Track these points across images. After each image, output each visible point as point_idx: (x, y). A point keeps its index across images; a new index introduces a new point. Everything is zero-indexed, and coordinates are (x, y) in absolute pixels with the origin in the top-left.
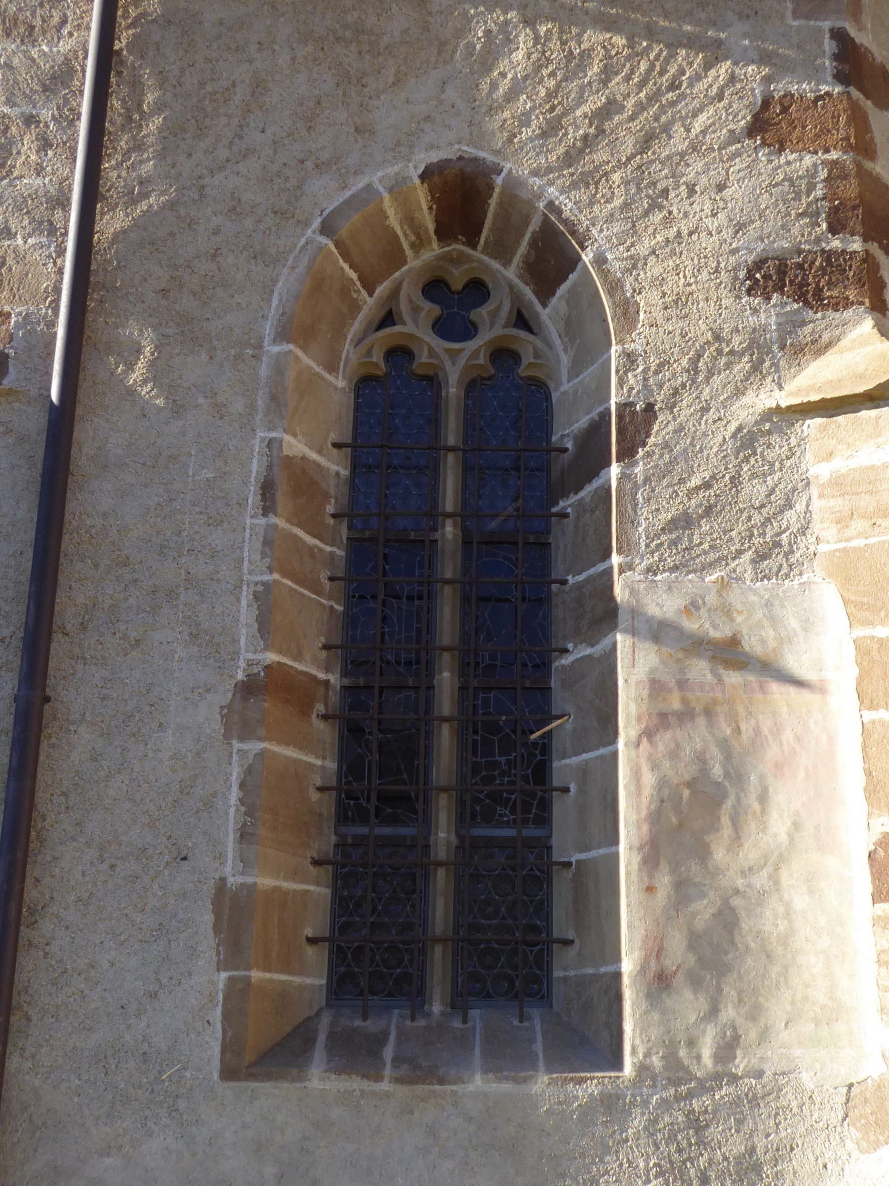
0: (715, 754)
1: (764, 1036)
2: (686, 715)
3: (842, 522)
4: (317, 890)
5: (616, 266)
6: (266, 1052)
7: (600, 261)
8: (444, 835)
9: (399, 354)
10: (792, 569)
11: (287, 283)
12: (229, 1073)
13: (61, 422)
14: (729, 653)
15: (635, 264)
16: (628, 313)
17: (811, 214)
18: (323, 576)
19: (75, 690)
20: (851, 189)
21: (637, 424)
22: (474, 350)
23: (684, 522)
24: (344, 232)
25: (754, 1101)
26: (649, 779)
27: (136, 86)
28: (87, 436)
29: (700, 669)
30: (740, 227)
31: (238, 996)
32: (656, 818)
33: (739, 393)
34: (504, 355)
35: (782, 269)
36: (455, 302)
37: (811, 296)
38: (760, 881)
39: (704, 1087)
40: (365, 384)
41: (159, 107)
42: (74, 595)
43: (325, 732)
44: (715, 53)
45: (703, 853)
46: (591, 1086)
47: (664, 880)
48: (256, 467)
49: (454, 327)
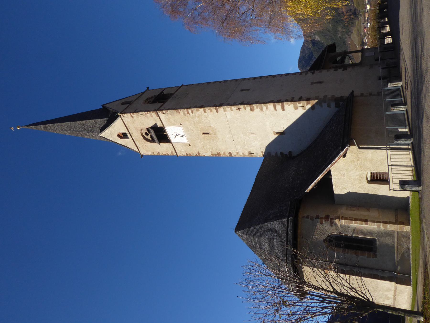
6: (375, 256)
13: (340, 264)
16: (333, 233)
29: (355, 232)
34: (334, 239)
44: (316, 226)
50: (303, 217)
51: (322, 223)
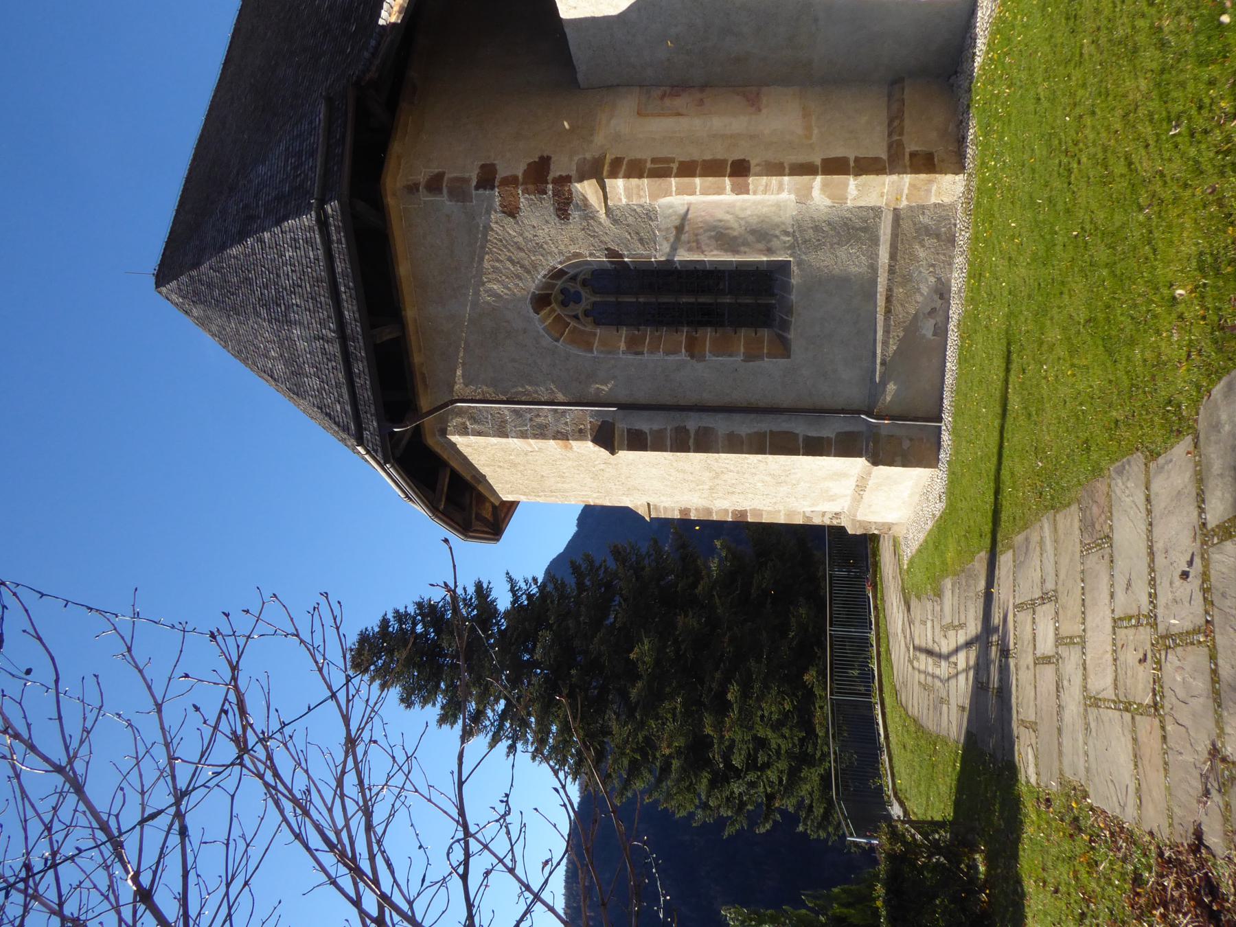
0: (708, 234)
1: (783, 223)
2: (697, 242)
3: (640, 197)
4: (743, 332)
5: (562, 258)
6: (783, 347)
7: (561, 263)
8: (728, 300)
9: (586, 314)
10: (654, 209)
11: (574, 350)
12: (789, 357)
13: (622, 406)
14: (680, 229)
15: (561, 253)
16: (576, 255)
17: (541, 200)
18: (657, 334)
19: (692, 398)
20: (531, 187)
21: (611, 253)
22: (584, 293)
23: (641, 240)
24: (557, 335)
25: (800, 227)
26: (715, 252)
27: (517, 393)
28: (623, 397)
29: (684, 237)
30: (547, 222)
31: (770, 355)
32: (726, 251)
33: (600, 223)
34: (584, 283)
35: (559, 209)
36: (568, 297)
37: (569, 201)
38: (743, 223)
39: (796, 240)
40: (597, 323)
41: (523, 386)
42: (666, 399)
43: (701, 331)
44: (487, 228)
45: (735, 238)
46: (794, 268)
47: (742, 249)
48: (630, 357)
49: (577, 298)
50: (413, 188)
51: (512, 212)
